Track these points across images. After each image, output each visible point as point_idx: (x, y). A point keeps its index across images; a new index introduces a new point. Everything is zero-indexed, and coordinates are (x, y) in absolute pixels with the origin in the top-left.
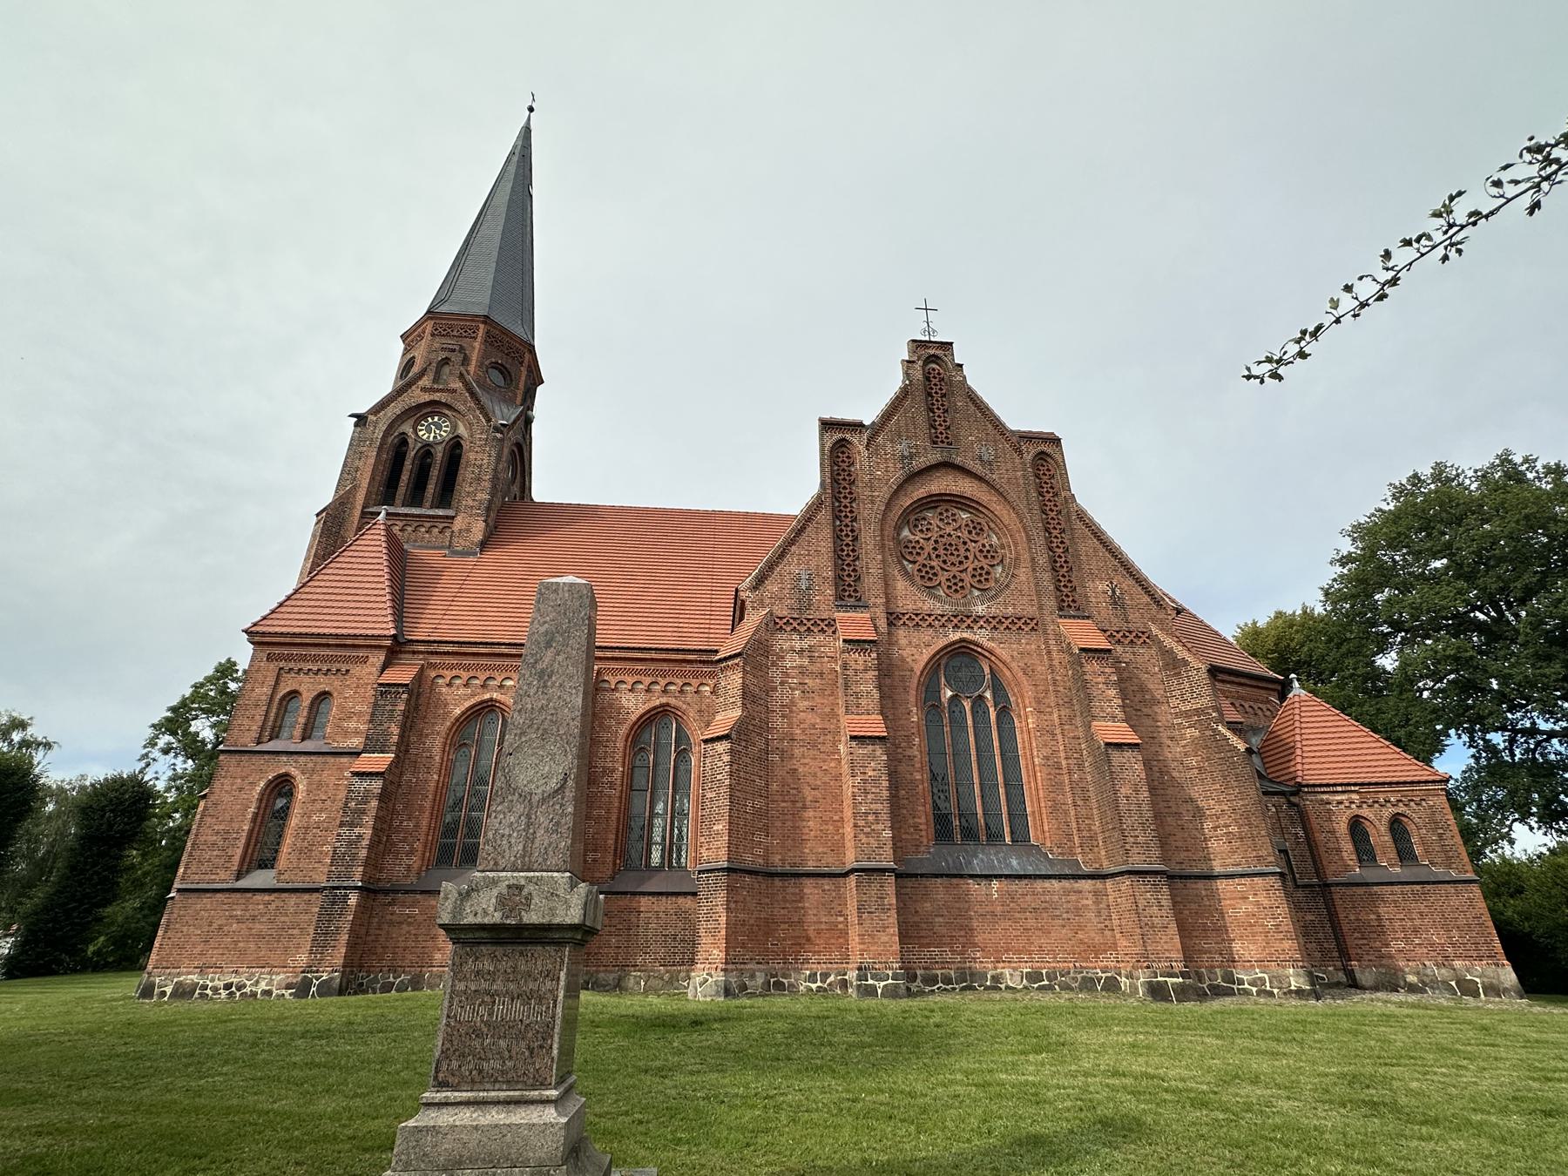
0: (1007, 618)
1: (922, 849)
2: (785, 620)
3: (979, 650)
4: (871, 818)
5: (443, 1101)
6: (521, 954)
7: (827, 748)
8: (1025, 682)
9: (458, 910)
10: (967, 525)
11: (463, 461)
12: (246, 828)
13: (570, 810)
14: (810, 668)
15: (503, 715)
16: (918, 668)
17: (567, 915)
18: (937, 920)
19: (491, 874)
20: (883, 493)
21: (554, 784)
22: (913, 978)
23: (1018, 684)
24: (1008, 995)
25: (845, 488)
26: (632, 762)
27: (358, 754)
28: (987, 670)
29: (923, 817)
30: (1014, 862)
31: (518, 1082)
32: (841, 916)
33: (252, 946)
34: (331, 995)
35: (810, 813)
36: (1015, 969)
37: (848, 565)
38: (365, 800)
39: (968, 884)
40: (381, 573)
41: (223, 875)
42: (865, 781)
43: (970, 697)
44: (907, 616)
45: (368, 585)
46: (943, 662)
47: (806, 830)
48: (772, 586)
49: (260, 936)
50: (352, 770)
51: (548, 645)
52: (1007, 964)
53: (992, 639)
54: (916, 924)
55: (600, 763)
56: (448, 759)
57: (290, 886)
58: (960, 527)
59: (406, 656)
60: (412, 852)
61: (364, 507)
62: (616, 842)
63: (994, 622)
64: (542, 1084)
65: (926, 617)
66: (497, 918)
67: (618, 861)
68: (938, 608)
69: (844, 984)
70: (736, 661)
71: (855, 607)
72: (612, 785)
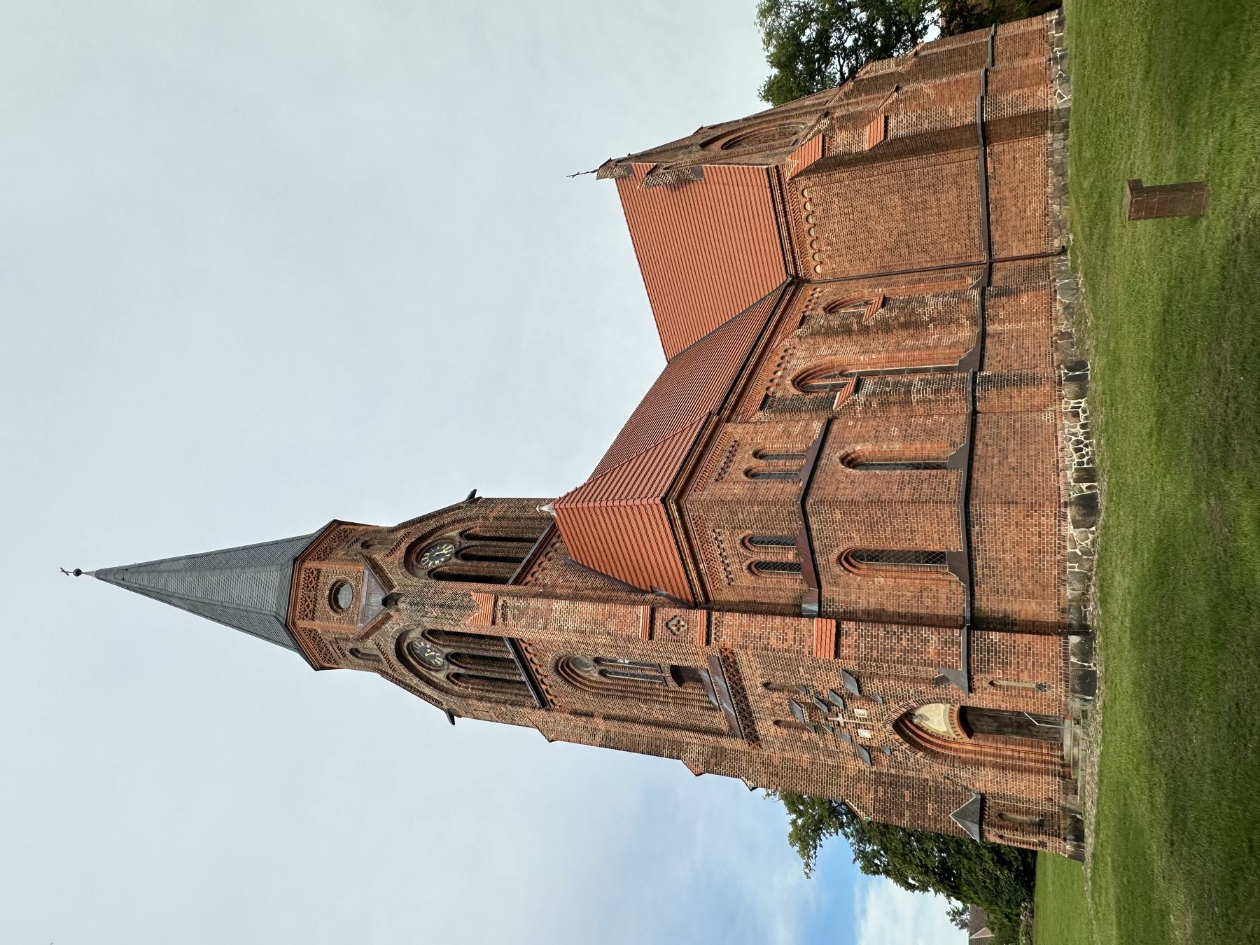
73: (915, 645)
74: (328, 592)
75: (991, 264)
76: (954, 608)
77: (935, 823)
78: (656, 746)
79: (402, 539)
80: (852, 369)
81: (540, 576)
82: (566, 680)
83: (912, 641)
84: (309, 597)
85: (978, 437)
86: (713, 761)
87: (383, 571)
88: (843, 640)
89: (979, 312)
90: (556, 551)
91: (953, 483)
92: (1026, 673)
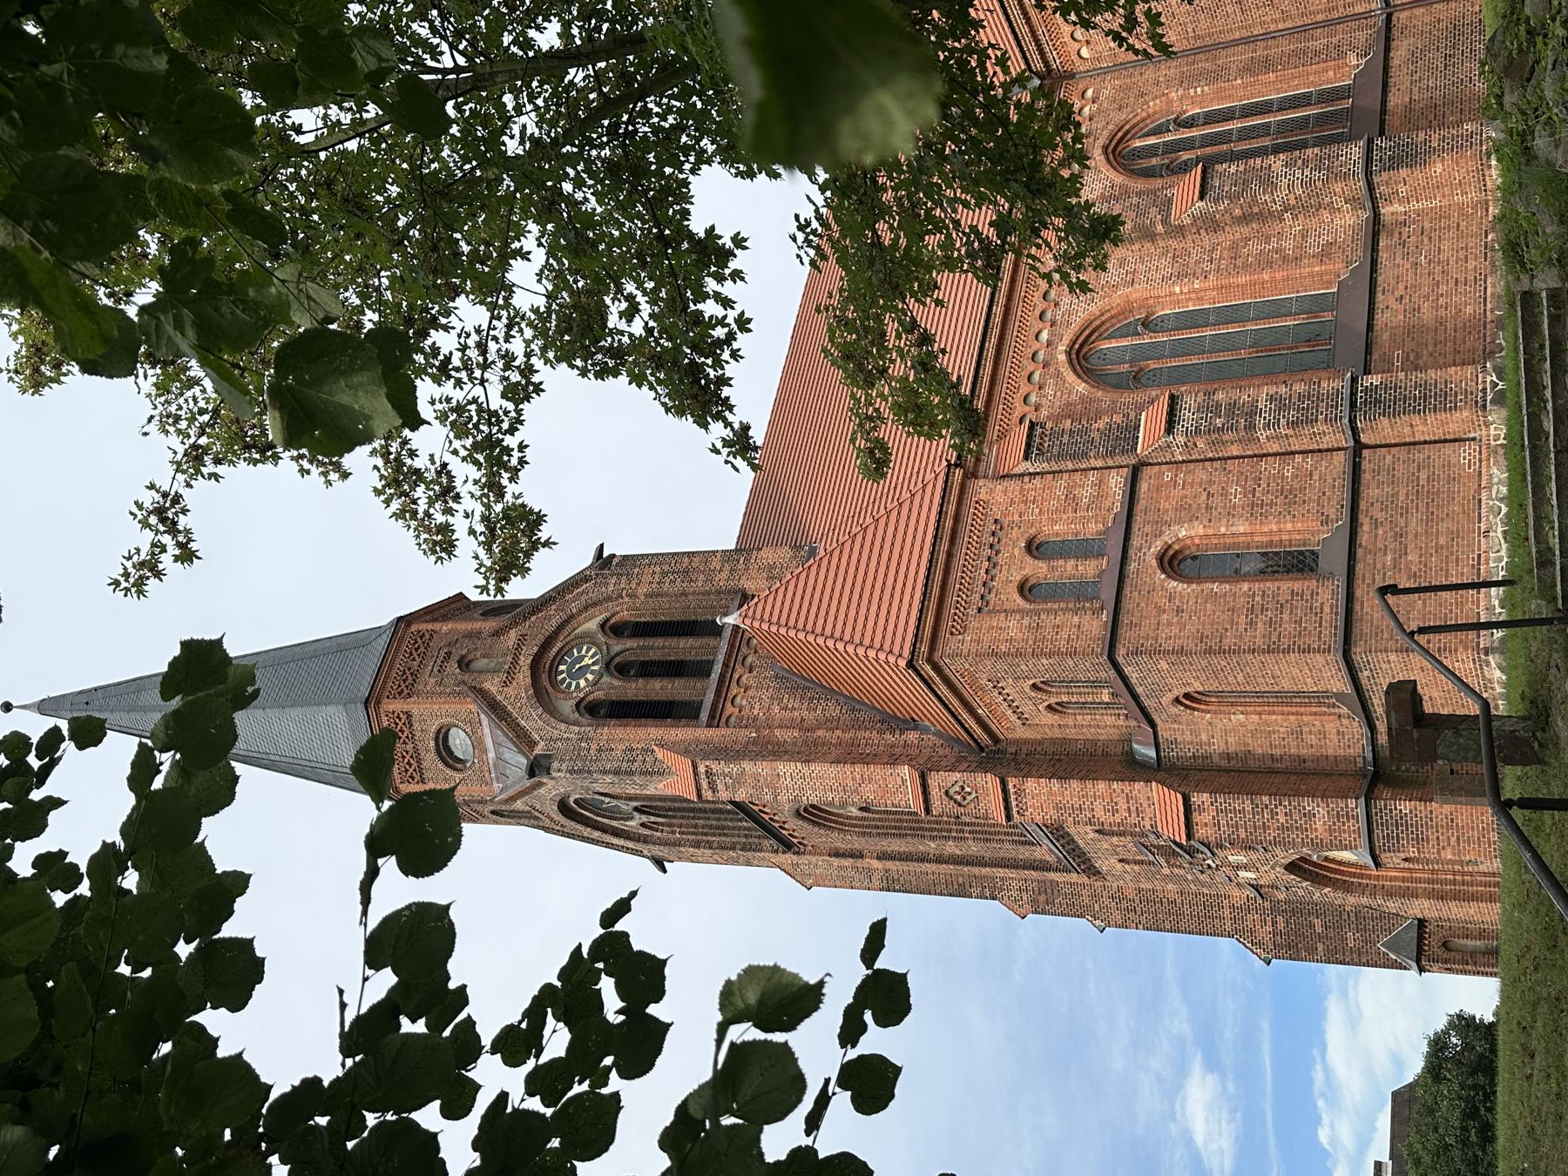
33: (1443, 526)
45: (852, 614)
70: (1010, 786)
73: (1296, 821)
74: (432, 743)
75: (1389, 16)
76: (1349, 746)
77: (1359, 956)
78: (960, 885)
79: (518, 648)
80: (1163, 309)
81: (744, 702)
82: (815, 823)
83: (1291, 816)
84: (407, 752)
85: (1363, 505)
86: (1042, 898)
87: (509, 714)
88: (1196, 817)
89: (1365, 191)
90: (756, 652)
91: (1327, 609)
92: (1449, 850)
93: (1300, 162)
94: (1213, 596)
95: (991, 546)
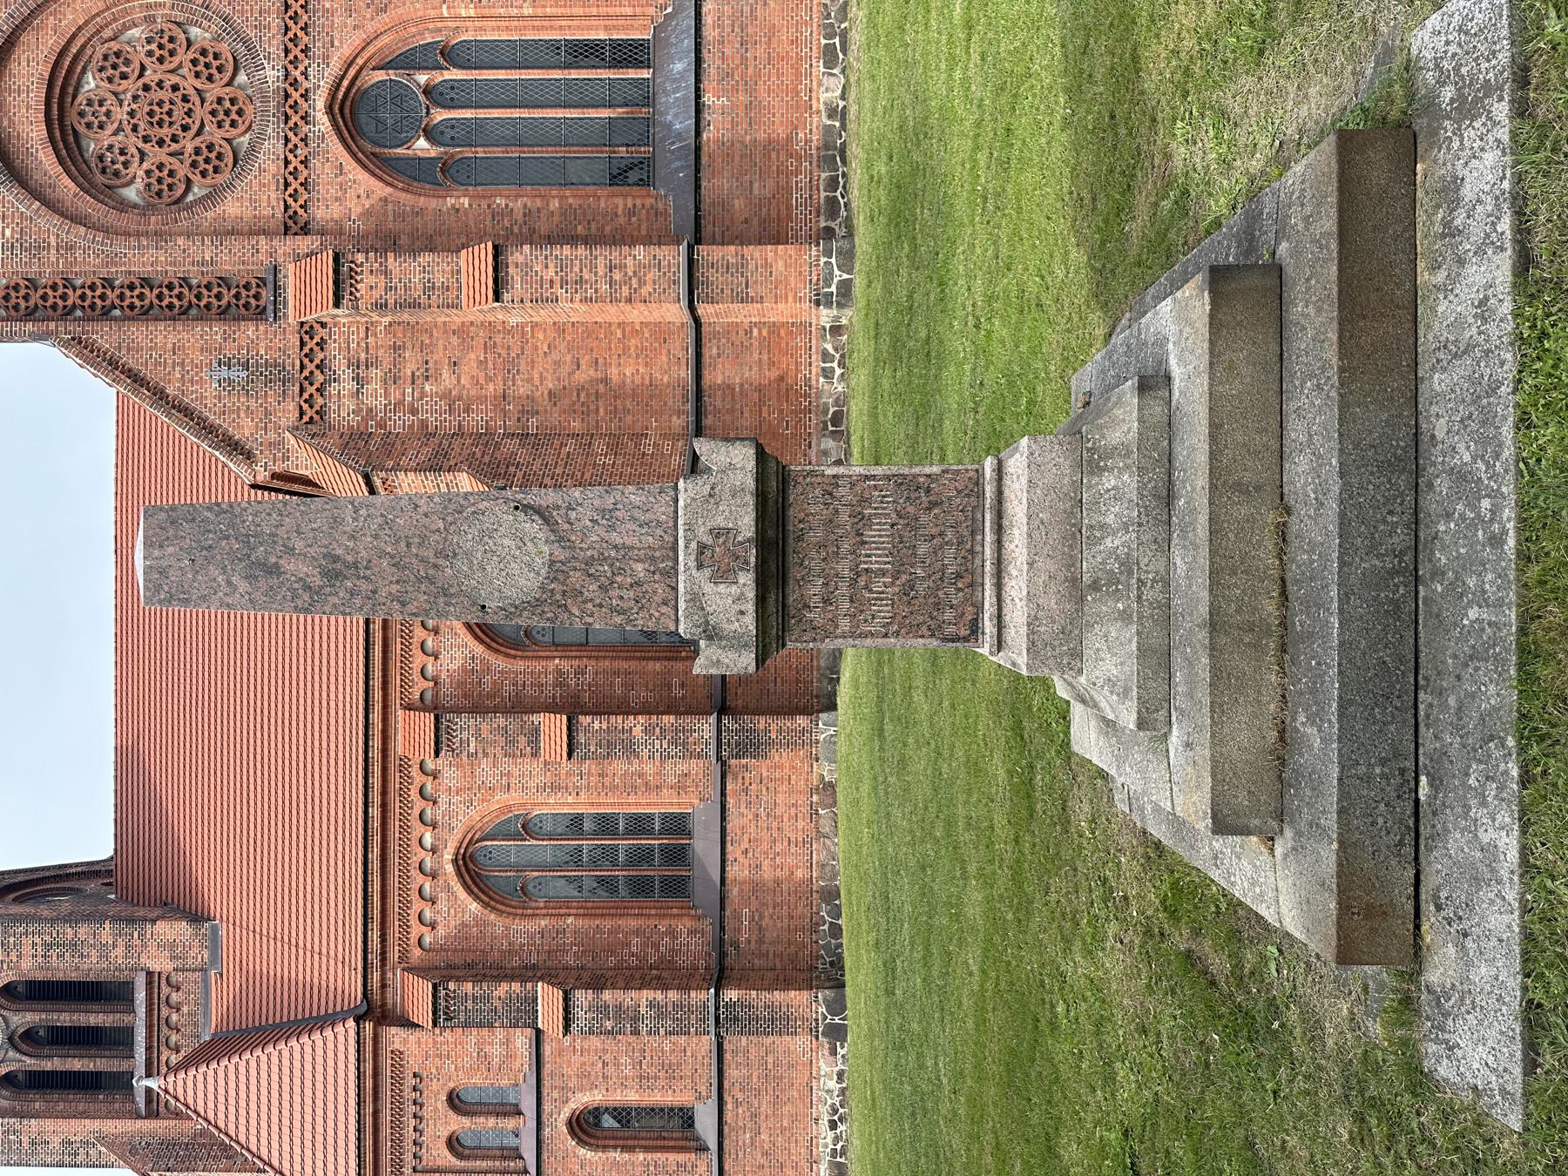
0: (287, 29)
1: (661, 206)
2: (305, 406)
3: (346, 83)
4: (617, 276)
5: (995, 621)
6: (800, 539)
7: (514, 342)
8: (400, 11)
9: (736, 642)
10: (110, 80)
11: (40, 976)
12: (641, 1156)
13: (577, 494)
14: (386, 365)
15: (479, 840)
16: (381, 190)
17: (743, 468)
18: (756, 192)
19: (682, 605)
20: (49, 226)
21: (532, 527)
22: (829, 233)
23: (403, 23)
24: (852, 95)
25: (44, 297)
26: (546, 647)
27: (539, 1032)
28: (380, 76)
29: (618, 203)
30: (679, 67)
31: (973, 519)
32: (751, 332)
33: (786, 1109)
34: (844, 996)
35: (613, 373)
36: (820, 84)
37: (199, 297)
38: (603, 1010)
39: (709, 139)
40: (253, 1064)
41: (702, 1168)
42: (564, 282)
43: (428, 108)
44: (290, 201)
46: (369, 147)
47: (638, 380)
48: (244, 429)
49: (775, 1103)
50: (561, 1036)
51: (274, 570)
52: (814, 94)
53: (326, 58)
54: (762, 222)
55: (549, 691)
56: (545, 908)
57: (715, 1081)
58: (115, 94)
59: (389, 996)
60: (672, 933)
61: (139, 1117)
62: (658, 659)
63: (296, 51)
64: (977, 484)
65: (291, 168)
66: (747, 579)
67: (683, 654)
68: (272, 148)
69: (836, 330)
71: (276, 287)
72: (580, 672)
85: (726, 1084)
93: (658, 730)
94: (615, 1163)
95: (415, 1103)
